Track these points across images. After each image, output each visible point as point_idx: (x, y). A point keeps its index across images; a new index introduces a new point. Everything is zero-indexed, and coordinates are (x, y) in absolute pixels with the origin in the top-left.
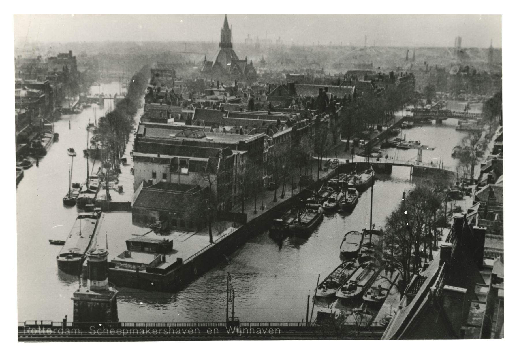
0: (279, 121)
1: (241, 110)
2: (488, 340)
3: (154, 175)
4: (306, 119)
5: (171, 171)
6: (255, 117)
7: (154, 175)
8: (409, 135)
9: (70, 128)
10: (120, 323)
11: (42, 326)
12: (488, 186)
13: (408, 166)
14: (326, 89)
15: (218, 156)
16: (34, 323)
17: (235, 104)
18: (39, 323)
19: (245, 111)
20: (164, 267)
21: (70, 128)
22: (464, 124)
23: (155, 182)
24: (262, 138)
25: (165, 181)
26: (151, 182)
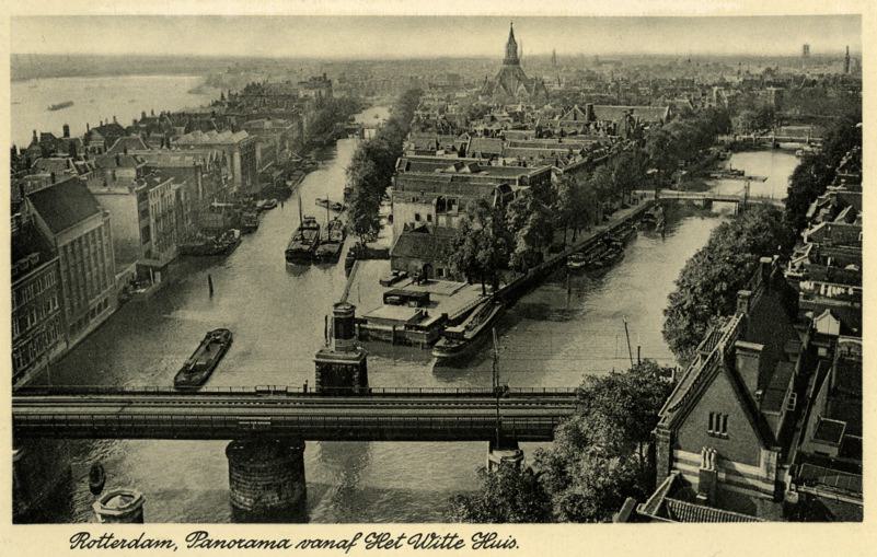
0: (571, 150)
1: (526, 139)
2: (864, 443)
3: (418, 217)
4: (521, 246)
5: (437, 212)
6: (541, 145)
7: (418, 217)
8: (737, 161)
9: (55, 108)
10: (371, 389)
11: (276, 393)
12: (823, 224)
13: (732, 201)
14: (632, 110)
15: (493, 194)
16: (266, 388)
17: (519, 131)
18: (272, 389)
19: (530, 140)
20: (426, 323)
21: (55, 108)
22: (647, 192)
23: (418, 225)
24: (550, 171)
25: (430, 224)
26: (413, 225)
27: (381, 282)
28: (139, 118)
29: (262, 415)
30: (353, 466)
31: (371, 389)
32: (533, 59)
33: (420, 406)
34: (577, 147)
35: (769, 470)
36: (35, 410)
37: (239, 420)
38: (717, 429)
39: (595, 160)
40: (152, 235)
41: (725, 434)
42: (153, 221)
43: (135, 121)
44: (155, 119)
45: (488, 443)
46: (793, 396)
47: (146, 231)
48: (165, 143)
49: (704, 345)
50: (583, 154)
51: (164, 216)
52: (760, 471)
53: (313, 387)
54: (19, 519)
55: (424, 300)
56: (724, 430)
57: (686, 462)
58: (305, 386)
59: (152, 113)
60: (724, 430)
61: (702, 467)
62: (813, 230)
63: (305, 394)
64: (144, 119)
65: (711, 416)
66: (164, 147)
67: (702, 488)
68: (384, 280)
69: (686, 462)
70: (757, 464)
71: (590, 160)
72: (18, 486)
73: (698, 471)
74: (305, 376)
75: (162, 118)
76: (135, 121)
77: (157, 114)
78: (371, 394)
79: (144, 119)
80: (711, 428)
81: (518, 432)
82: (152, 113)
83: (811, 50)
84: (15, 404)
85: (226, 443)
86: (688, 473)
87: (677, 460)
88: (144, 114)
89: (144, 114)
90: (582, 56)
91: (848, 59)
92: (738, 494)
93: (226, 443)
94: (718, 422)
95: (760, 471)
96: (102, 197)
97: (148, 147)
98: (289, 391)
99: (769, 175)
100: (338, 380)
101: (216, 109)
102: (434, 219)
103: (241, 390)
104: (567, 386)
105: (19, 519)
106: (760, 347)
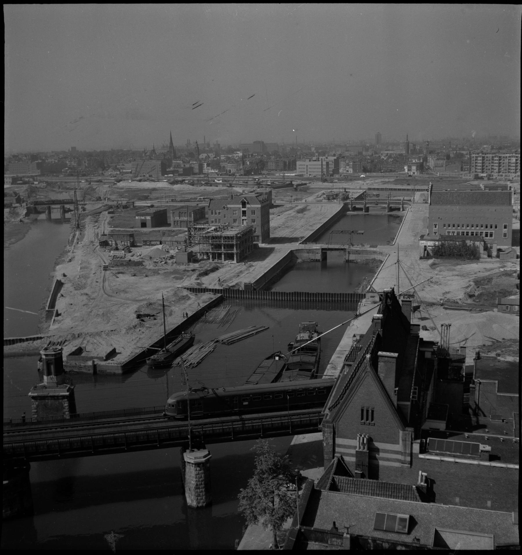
23: (358, 338)
35: (405, 446)
38: (367, 419)
46: (415, 389)
52: (399, 447)
60: (372, 420)
61: (357, 449)
63: (24, 422)
67: (358, 465)
69: (345, 447)
70: (396, 442)
72: (237, 541)
73: (355, 453)
80: (362, 419)
86: (348, 455)
87: (377, 450)
90: (262, 144)
91: (408, 144)
94: (367, 415)
95: (399, 447)
96: (167, 328)
98: (13, 422)
106: (396, 355)
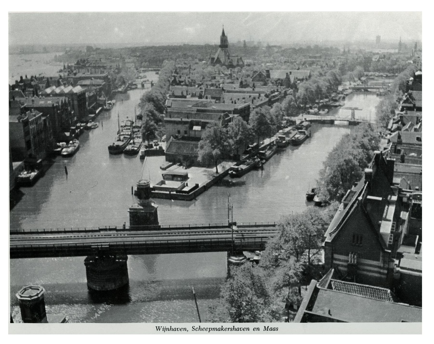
7: (179, 132)
10: (160, 226)
18: (108, 228)
27: (161, 168)
28: (19, 80)
29: (104, 241)
30: (150, 267)
31: (160, 226)
32: (233, 45)
33: (210, 233)
34: (263, 92)
36: (136, 239)
37: (91, 245)
39: (272, 100)
40: (32, 145)
41: (361, 245)
42: (32, 137)
43: (17, 81)
44: (28, 80)
45: (226, 252)
47: (28, 143)
48: (35, 93)
49: (346, 198)
50: (267, 96)
51: (38, 134)
53: (128, 226)
54: (421, 333)
55: (185, 178)
56: (361, 243)
57: (339, 260)
58: (124, 225)
59: (26, 76)
62: (392, 136)
63: (124, 230)
64: (22, 80)
65: (354, 236)
66: (35, 96)
68: (162, 167)
69: (339, 260)
71: (270, 100)
74: (124, 220)
75: (32, 80)
76: (17, 81)
77: (29, 77)
78: (159, 228)
79: (22, 80)
80: (353, 242)
81: (243, 246)
82: (26, 76)
83: (381, 38)
84: (12, 240)
85: (85, 257)
88: (21, 77)
89: (21, 77)
92: (368, 275)
93: (85, 257)
97: (26, 96)
99: (366, 107)
100: (143, 219)
101: (62, 74)
102: (188, 132)
103: (175, 227)
104: (105, 225)
105: (421, 333)
